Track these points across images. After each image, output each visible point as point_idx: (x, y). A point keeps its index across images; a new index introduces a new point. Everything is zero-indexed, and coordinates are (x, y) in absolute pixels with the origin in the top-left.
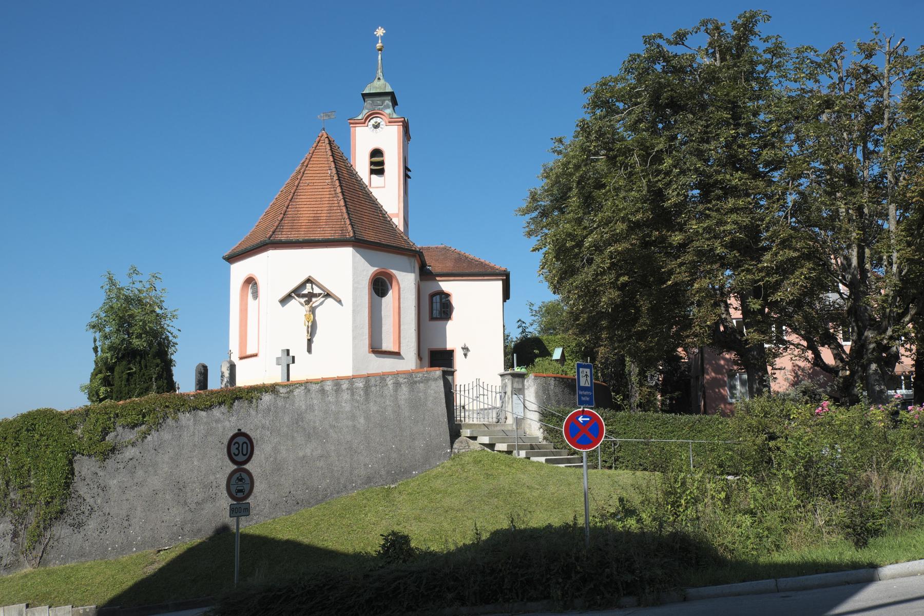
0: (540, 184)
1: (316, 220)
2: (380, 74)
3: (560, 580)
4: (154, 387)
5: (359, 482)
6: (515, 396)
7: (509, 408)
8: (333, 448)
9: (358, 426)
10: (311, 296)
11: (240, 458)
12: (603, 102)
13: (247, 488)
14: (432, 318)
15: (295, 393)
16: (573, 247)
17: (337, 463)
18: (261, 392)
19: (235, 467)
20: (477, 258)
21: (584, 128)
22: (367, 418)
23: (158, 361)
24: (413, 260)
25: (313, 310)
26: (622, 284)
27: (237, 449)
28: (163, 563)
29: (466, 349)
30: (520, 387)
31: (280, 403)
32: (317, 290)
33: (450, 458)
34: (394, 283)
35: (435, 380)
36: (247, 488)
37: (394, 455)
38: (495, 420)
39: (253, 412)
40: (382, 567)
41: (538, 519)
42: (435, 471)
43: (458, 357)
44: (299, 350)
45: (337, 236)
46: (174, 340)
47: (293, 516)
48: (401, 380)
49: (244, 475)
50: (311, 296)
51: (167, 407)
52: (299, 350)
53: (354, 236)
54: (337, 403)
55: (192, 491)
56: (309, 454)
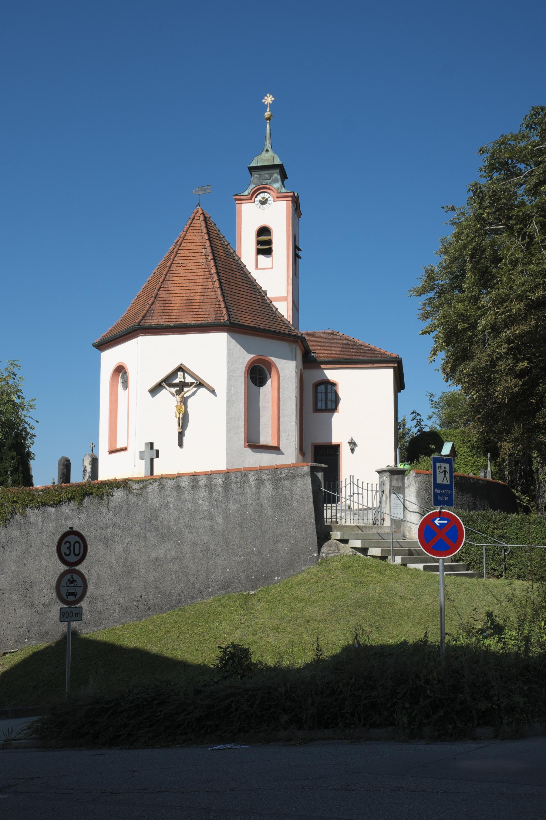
0: (436, 261)
1: (189, 303)
2: (268, 145)
3: (407, 705)
4: (10, 481)
5: (216, 587)
6: (393, 496)
7: (386, 510)
8: (188, 550)
9: (216, 526)
10: (183, 385)
11: (72, 559)
12: (501, 163)
13: (79, 591)
14: (317, 410)
15: (149, 490)
16: (465, 330)
17: (192, 566)
18: (112, 488)
19: (66, 568)
20: (367, 344)
21: (478, 193)
22: (226, 517)
23: (14, 454)
24: (294, 345)
25: (184, 401)
26: (521, 370)
27: (69, 548)
28: (7, 667)
29: (353, 444)
30: (400, 485)
31: (133, 500)
32: (189, 379)
33: (317, 563)
34: (273, 372)
35: (303, 476)
36: (79, 591)
37: (255, 559)
38: (371, 522)
39: (104, 510)
40: (216, 683)
41: (391, 635)
42: (300, 577)
43: (345, 451)
44: (166, 442)
45: (210, 321)
46: (32, 432)
47: (144, 622)
48: (265, 477)
49: (76, 577)
50: (183, 385)
51: (16, 502)
52: (166, 442)
53: (229, 320)
54: (194, 500)
55: (40, 591)
56: (162, 556)
